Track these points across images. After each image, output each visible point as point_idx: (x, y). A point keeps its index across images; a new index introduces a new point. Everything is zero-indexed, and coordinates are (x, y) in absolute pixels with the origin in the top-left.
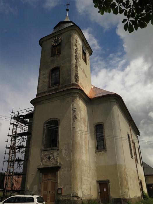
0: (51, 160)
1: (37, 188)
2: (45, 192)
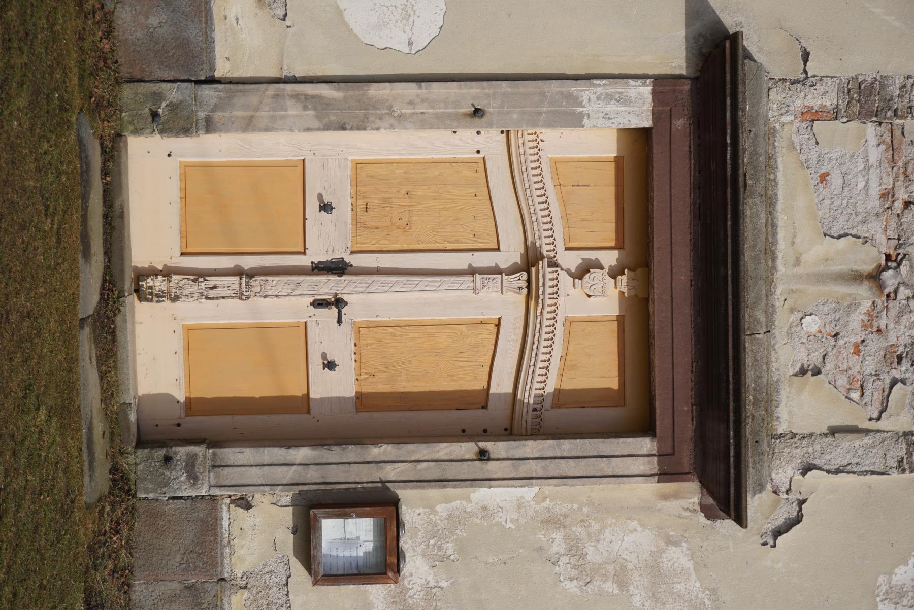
0: (857, 319)
1: (398, 42)
2: (326, 207)
